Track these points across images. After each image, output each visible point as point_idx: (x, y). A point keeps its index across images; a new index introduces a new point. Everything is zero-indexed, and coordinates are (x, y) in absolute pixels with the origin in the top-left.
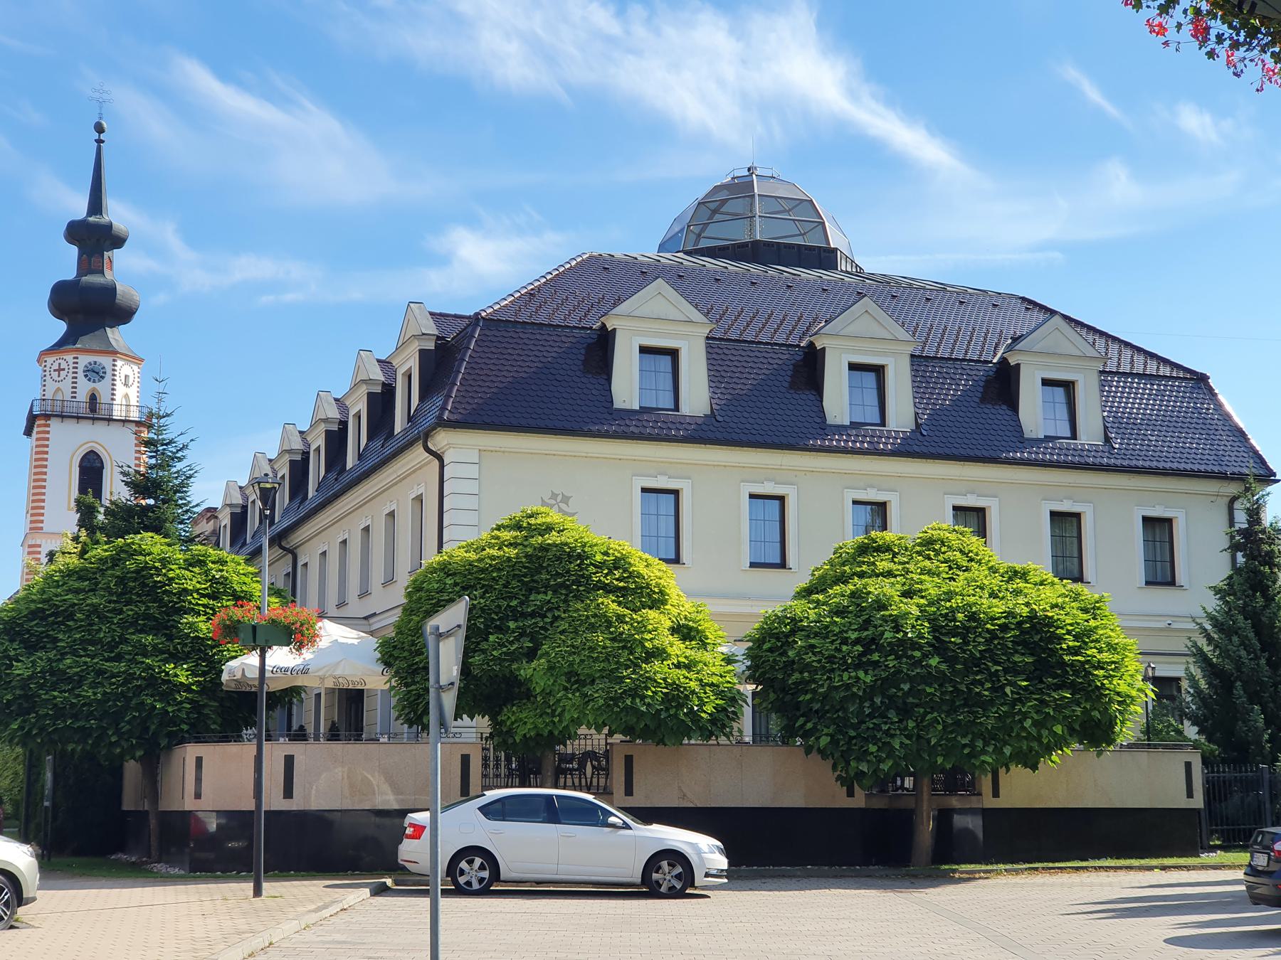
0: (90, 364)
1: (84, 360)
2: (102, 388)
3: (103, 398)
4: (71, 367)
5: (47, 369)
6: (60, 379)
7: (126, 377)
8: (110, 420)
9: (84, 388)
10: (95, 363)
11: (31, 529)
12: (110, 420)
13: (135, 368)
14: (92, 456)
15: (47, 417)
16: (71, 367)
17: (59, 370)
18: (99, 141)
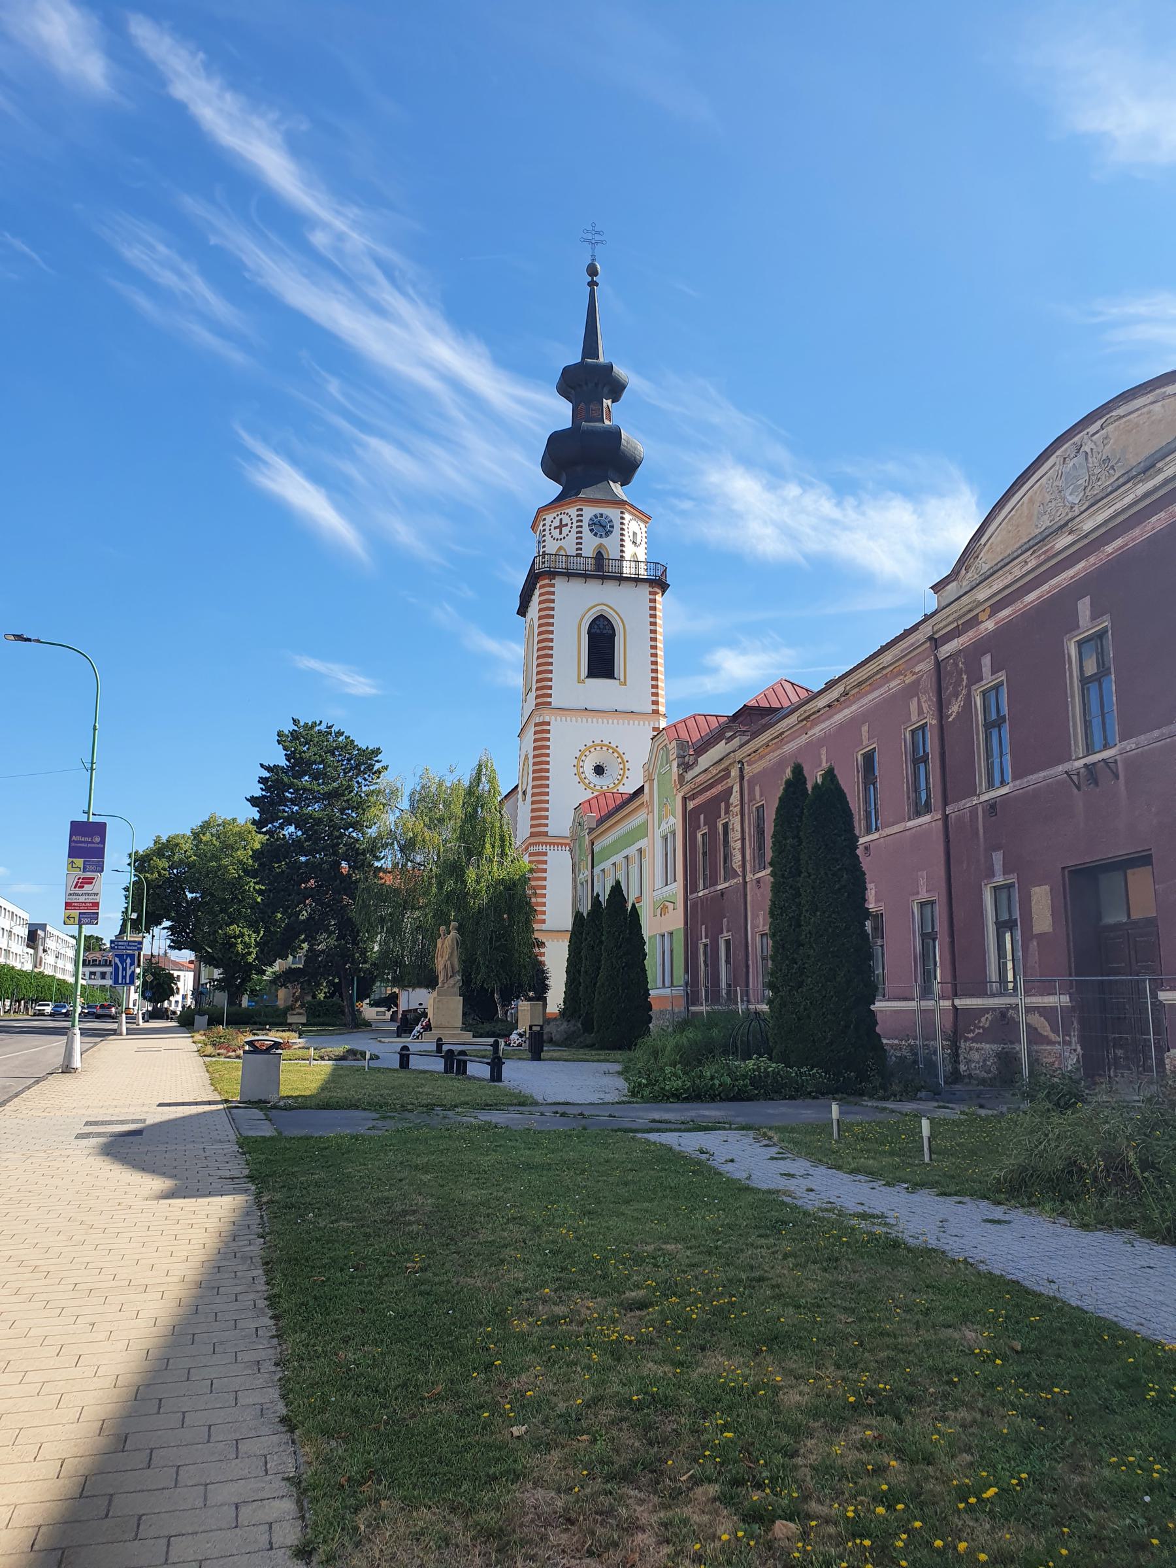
0: (596, 516)
1: (589, 512)
2: (610, 544)
3: (613, 553)
4: (574, 521)
5: (547, 527)
6: (562, 536)
7: (635, 534)
8: (620, 579)
9: (590, 544)
10: (601, 515)
11: (537, 705)
12: (620, 579)
13: (642, 525)
14: (601, 622)
15: (552, 574)
16: (574, 521)
17: (561, 526)
18: (592, 284)
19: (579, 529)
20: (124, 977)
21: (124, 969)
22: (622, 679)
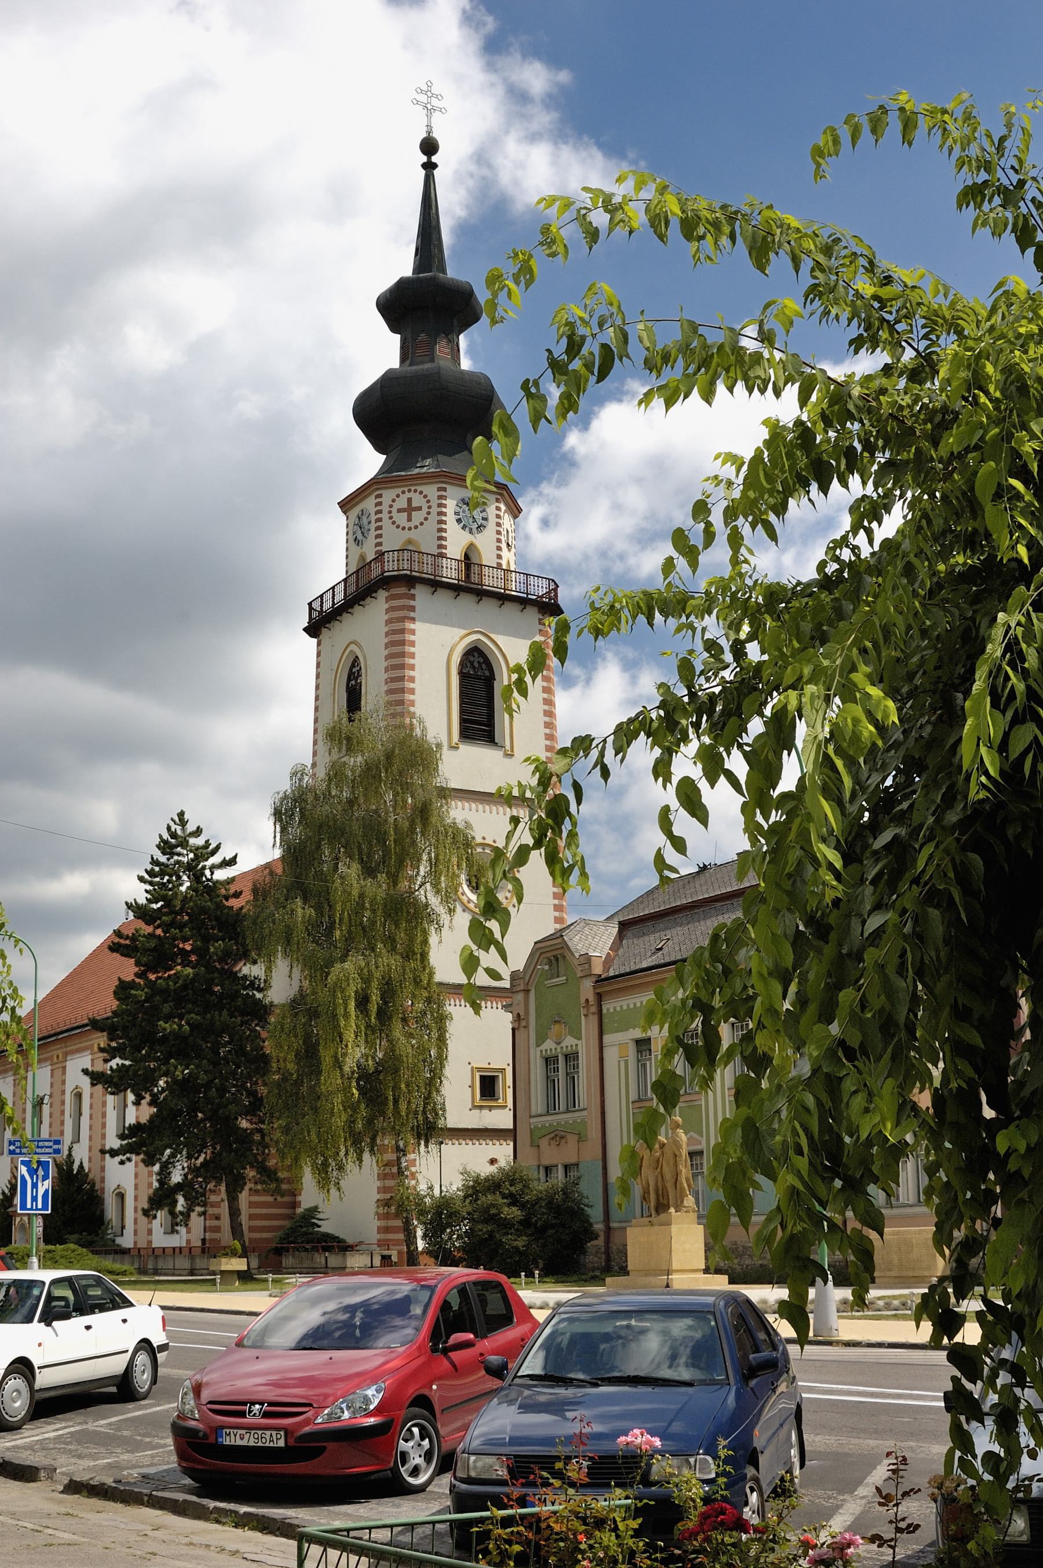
3: (488, 558)
18: (429, 167)
19: (379, 532)
20: (34, 1199)
21: (35, 1186)
22: (508, 747)
